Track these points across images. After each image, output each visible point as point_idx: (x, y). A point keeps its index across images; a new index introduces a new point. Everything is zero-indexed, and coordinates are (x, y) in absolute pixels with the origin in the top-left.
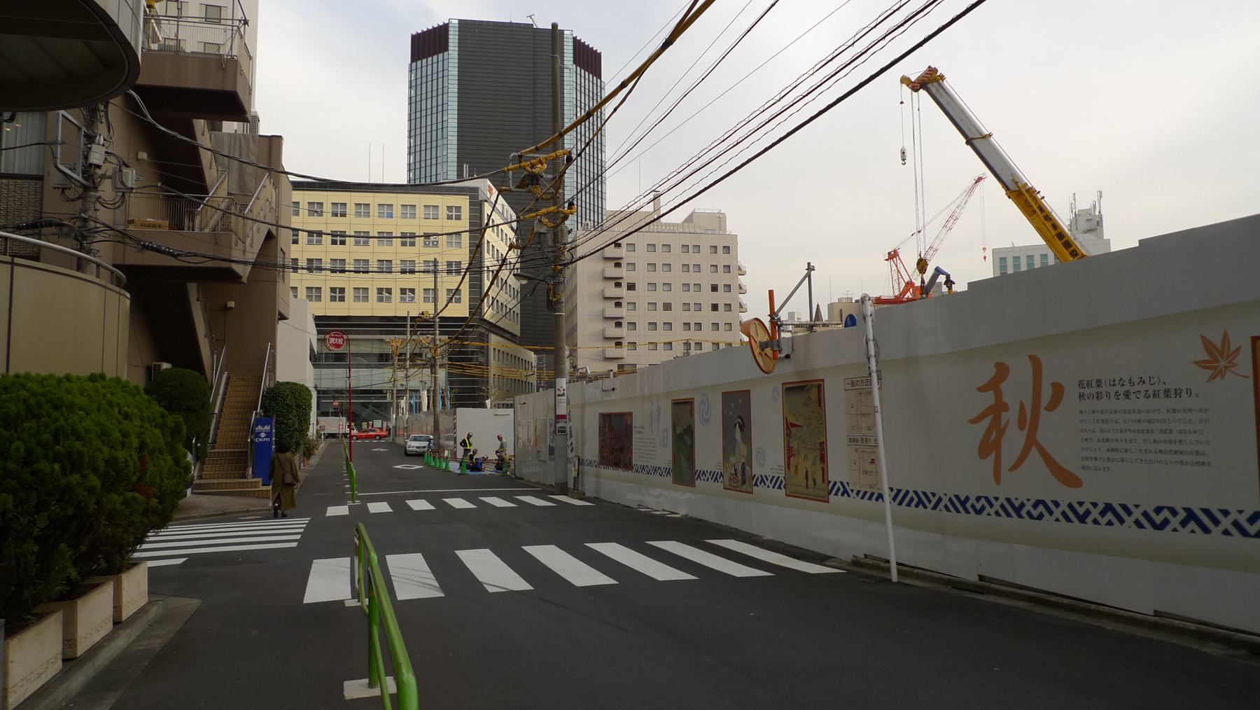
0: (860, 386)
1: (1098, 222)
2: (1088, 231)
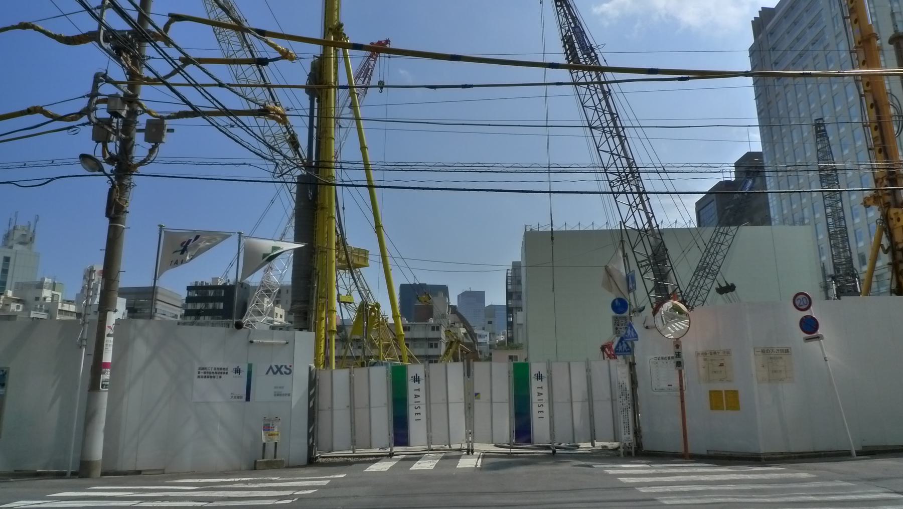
1: (31, 238)
2: (21, 243)
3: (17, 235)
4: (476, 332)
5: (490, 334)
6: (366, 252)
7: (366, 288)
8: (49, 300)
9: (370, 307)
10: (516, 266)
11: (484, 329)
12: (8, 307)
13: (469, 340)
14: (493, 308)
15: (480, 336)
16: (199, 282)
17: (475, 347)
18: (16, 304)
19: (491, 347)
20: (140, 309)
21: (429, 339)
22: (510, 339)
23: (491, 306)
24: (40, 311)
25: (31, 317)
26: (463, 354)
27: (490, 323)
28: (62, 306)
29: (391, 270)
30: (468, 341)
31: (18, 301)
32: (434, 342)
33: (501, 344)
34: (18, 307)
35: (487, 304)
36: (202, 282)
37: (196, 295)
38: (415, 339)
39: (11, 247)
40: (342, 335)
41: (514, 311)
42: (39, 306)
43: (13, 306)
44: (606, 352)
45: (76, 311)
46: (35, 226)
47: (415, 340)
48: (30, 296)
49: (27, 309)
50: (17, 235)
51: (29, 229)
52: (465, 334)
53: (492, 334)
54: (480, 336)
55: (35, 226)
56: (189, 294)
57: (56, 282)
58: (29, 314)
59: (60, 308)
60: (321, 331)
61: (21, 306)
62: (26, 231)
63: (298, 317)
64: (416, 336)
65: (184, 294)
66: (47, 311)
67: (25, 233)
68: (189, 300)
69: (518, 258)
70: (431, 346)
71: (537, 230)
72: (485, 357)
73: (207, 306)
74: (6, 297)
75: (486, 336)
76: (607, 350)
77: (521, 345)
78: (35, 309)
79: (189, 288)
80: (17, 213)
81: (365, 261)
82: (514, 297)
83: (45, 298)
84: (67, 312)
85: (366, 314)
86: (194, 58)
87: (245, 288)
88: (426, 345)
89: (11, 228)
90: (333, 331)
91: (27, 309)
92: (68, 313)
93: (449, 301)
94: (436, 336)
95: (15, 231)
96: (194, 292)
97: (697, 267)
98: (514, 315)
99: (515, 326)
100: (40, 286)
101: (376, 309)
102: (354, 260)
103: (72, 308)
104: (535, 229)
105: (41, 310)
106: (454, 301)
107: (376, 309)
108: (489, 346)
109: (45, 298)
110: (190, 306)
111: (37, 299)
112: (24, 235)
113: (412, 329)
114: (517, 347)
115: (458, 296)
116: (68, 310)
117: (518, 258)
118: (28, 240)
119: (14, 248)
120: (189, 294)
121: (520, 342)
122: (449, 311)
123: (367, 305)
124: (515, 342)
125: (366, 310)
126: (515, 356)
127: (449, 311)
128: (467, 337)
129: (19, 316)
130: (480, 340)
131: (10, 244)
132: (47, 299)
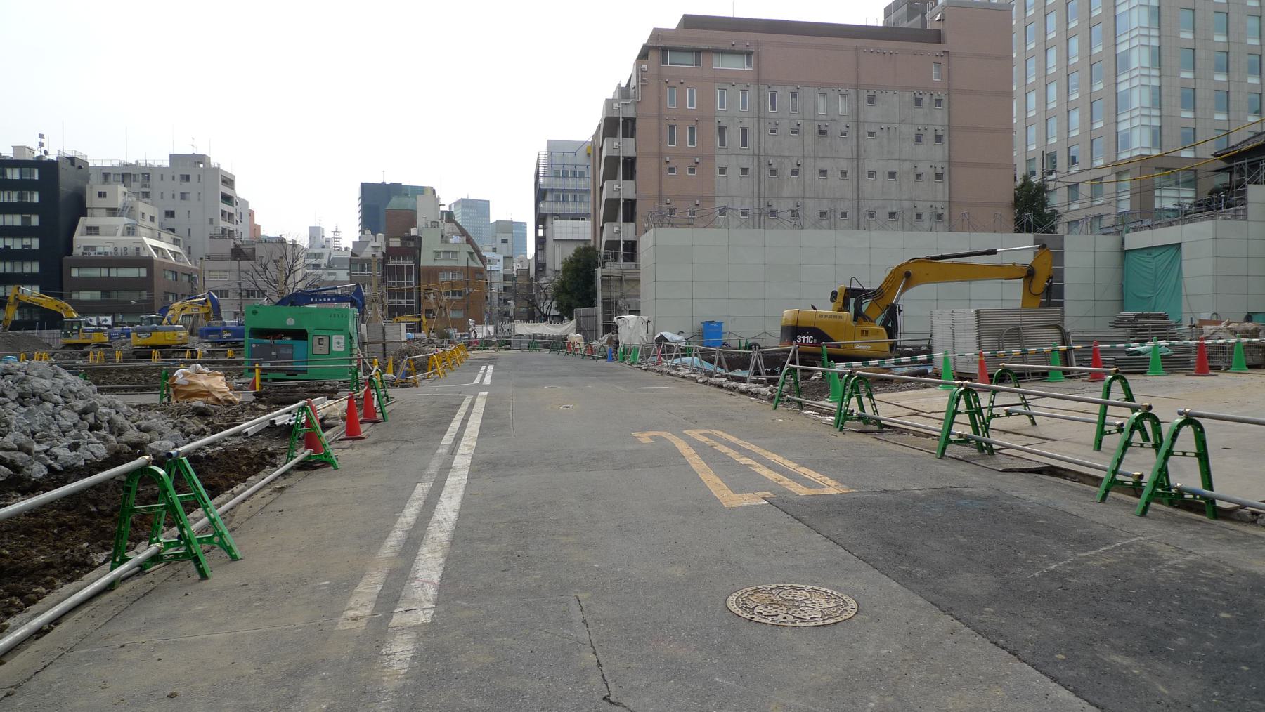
0: (391, 294)
5: (505, 258)
11: (494, 250)
13: (477, 263)
27: (505, 241)
30: (475, 265)
35: (492, 220)
41: (549, 220)
54: (489, 261)
75: (499, 261)
82: (549, 197)
87: (80, 167)
99: (549, 244)
128: (473, 259)
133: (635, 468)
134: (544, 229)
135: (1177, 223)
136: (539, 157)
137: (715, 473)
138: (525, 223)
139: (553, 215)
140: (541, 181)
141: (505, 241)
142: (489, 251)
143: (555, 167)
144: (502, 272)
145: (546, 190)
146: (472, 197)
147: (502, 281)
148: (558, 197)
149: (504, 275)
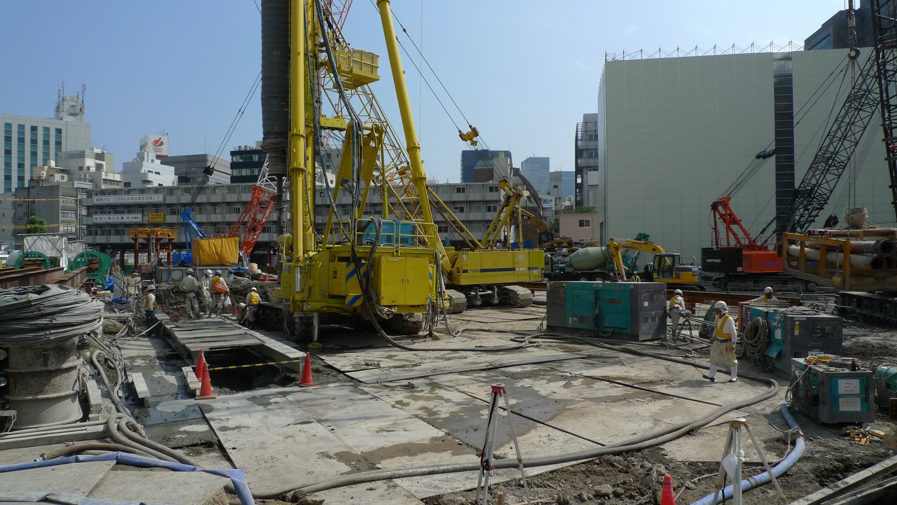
1: (81, 109)
2: (71, 114)
3: (67, 105)
4: (540, 196)
5: (556, 199)
6: (373, 57)
7: (383, 119)
8: (93, 169)
9: (366, 132)
10: (590, 122)
11: (549, 193)
12: (52, 177)
13: (532, 203)
14: (558, 175)
15: (545, 201)
16: (243, 146)
17: (539, 212)
18: (60, 175)
19: (557, 212)
20: (194, 178)
21: (487, 202)
22: (579, 203)
23: (556, 173)
24: (85, 181)
25: (75, 187)
26: (525, 219)
27: (556, 187)
28: (106, 175)
29: (404, 72)
30: (531, 205)
31: (63, 171)
32: (492, 205)
33: (568, 209)
34: (63, 178)
36: (240, 147)
37: (240, 160)
38: (470, 201)
39: (62, 119)
40: (349, 185)
41: (585, 172)
42: (83, 176)
43: (58, 177)
44: (719, 212)
45: (122, 180)
46: (83, 97)
47: (470, 202)
48: (74, 165)
49: (71, 180)
50: (67, 105)
51: (78, 99)
52: (528, 197)
53: (558, 199)
54: (545, 201)
55: (83, 97)
56: (234, 160)
57: (105, 152)
58: (73, 185)
59: (104, 177)
60: (587, 253)
61: (66, 176)
62: (75, 102)
63: (275, 157)
64: (471, 198)
65: (229, 159)
66: (91, 181)
67: (74, 104)
68: (234, 166)
69: (593, 107)
70: (489, 210)
71: (622, 59)
72: (550, 223)
73: (252, 172)
74: (50, 168)
76: (720, 208)
77: (593, 208)
78: (80, 179)
79: (233, 154)
80: (63, 83)
81: (372, 72)
82: (585, 154)
83: (88, 168)
84: (112, 182)
85: (358, 143)
86: (723, 467)
88: (484, 208)
89: (61, 99)
90: (299, 169)
91: (71, 180)
92: (113, 183)
93: (511, 162)
94: (495, 198)
95: (64, 102)
96: (238, 157)
97: (849, 96)
98: (585, 176)
99: (585, 188)
100: (82, 155)
101: (376, 135)
102: (354, 69)
103: (118, 178)
104: (619, 57)
105: (85, 180)
106: (517, 164)
107: (376, 135)
108: (554, 212)
109: (88, 168)
110: (236, 173)
111: (81, 168)
112: (73, 106)
113: (467, 190)
114: (589, 211)
115: (522, 163)
116: (112, 179)
117: (593, 107)
118: (77, 112)
119: (64, 120)
120: (234, 160)
121: (591, 205)
122: (511, 173)
123: (360, 127)
124: (585, 205)
125: (358, 136)
126: (586, 221)
127: (511, 173)
128: (530, 201)
129: (60, 186)
130: (545, 206)
131: (61, 116)
132: (91, 169)
133: (865, 314)
134: (582, 178)
135: (700, 499)
136: (577, 127)
137: (424, 444)
138: (463, 151)
139: (588, 167)
140: (579, 143)
141: (556, 187)
142: (545, 194)
143: (590, 133)
144: (554, 209)
145: (583, 149)
146: (537, 156)
147: (554, 214)
148: (591, 154)
149: (555, 211)
